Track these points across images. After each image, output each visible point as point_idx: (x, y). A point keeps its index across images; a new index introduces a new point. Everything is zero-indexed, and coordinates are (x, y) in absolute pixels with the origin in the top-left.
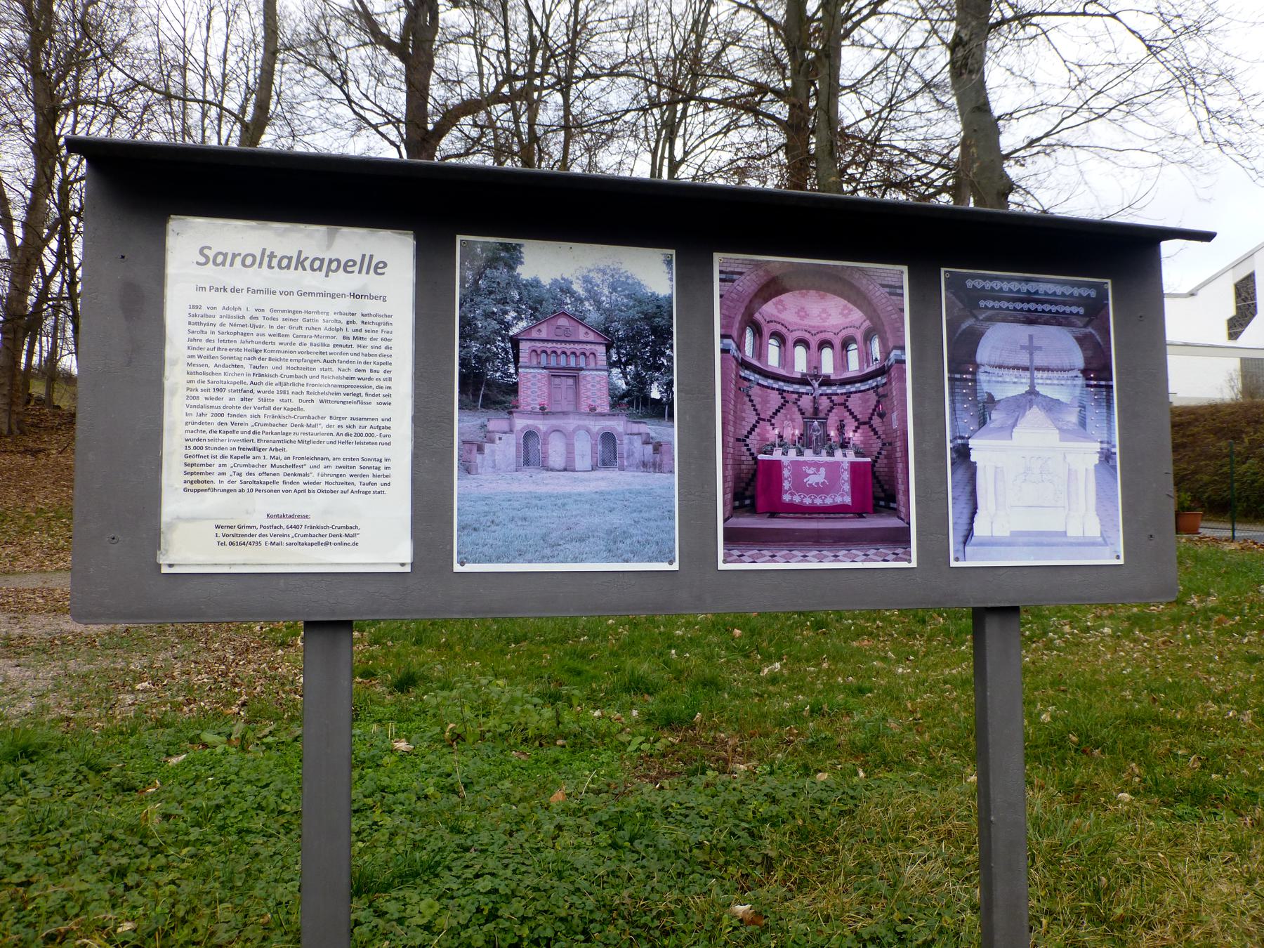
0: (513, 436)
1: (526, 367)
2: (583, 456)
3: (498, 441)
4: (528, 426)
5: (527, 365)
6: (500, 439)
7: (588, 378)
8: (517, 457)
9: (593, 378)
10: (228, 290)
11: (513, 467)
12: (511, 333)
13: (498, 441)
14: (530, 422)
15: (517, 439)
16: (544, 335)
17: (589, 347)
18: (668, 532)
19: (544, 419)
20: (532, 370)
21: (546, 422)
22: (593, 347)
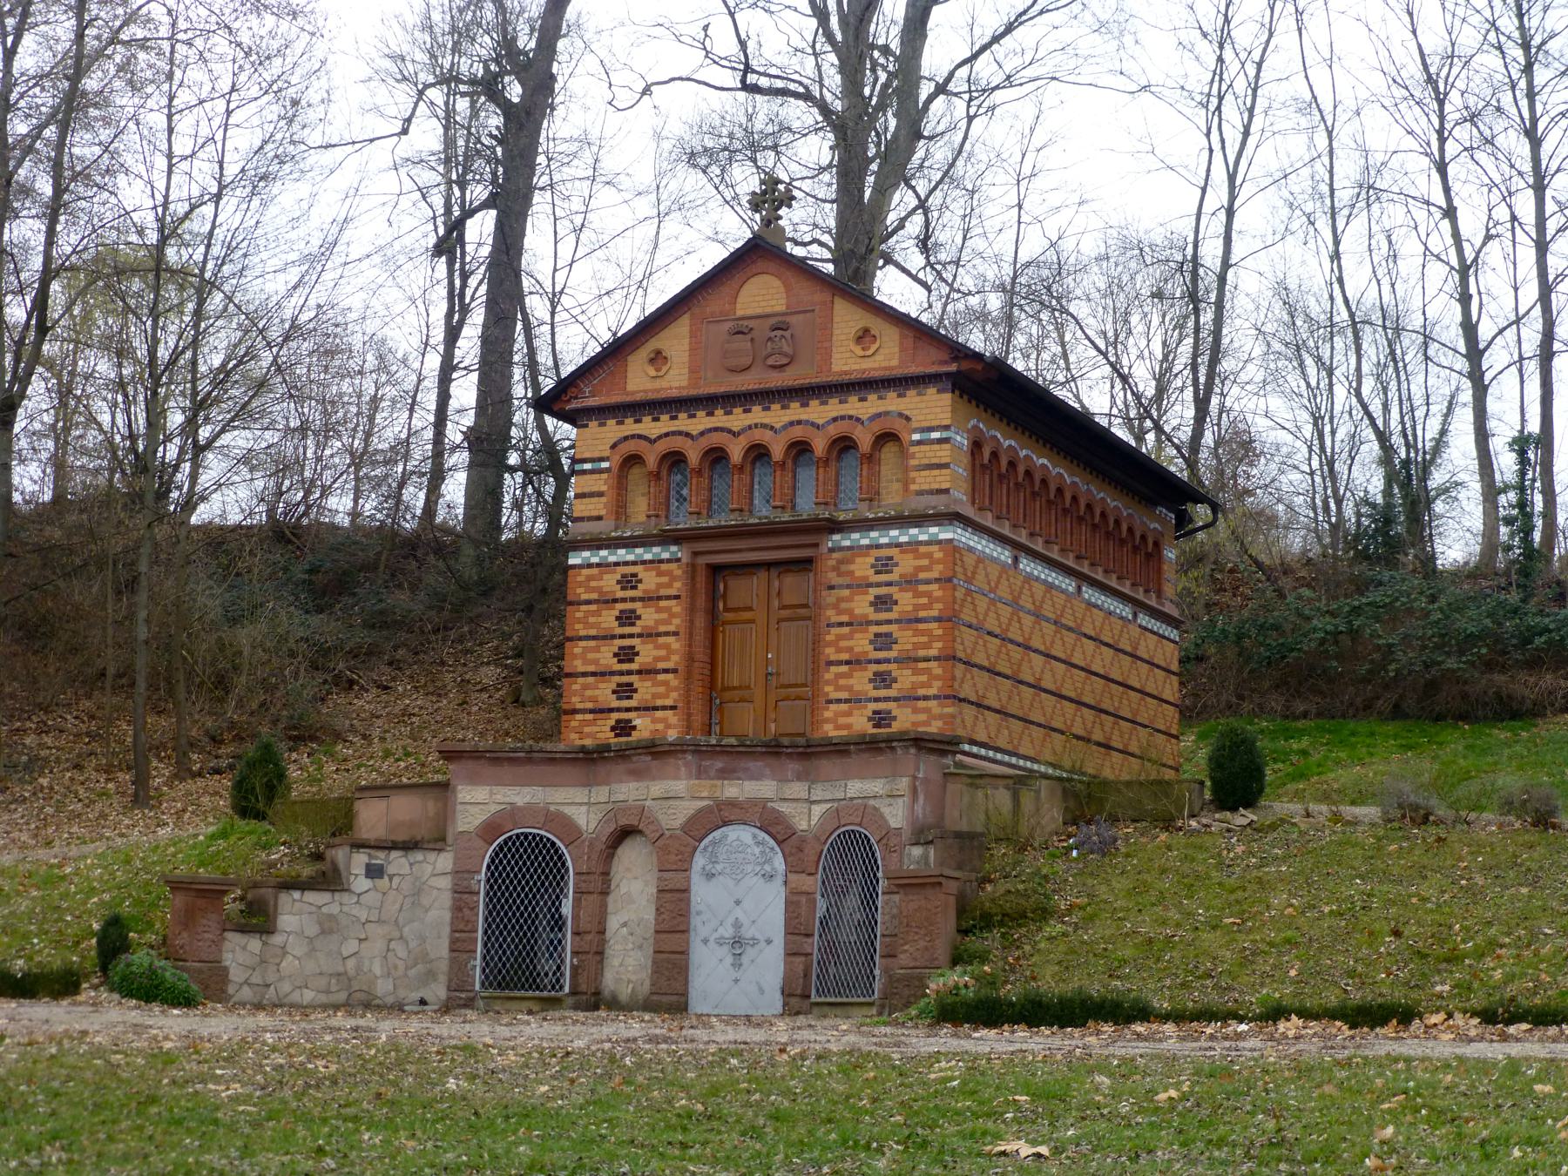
0: (445, 861)
1: (596, 543)
2: (738, 943)
3: (361, 883)
4: (513, 813)
5: (605, 528)
6: (374, 872)
7: (863, 568)
8: (459, 947)
9: (884, 565)
10: (738, 975)
11: (438, 992)
12: (194, 520)
13: (361, 883)
14: (521, 796)
15: (461, 873)
16: (676, 380)
17: (869, 406)
18: (472, 909)
19: (587, 784)
20: (622, 554)
21: (601, 794)
22: (892, 402)
